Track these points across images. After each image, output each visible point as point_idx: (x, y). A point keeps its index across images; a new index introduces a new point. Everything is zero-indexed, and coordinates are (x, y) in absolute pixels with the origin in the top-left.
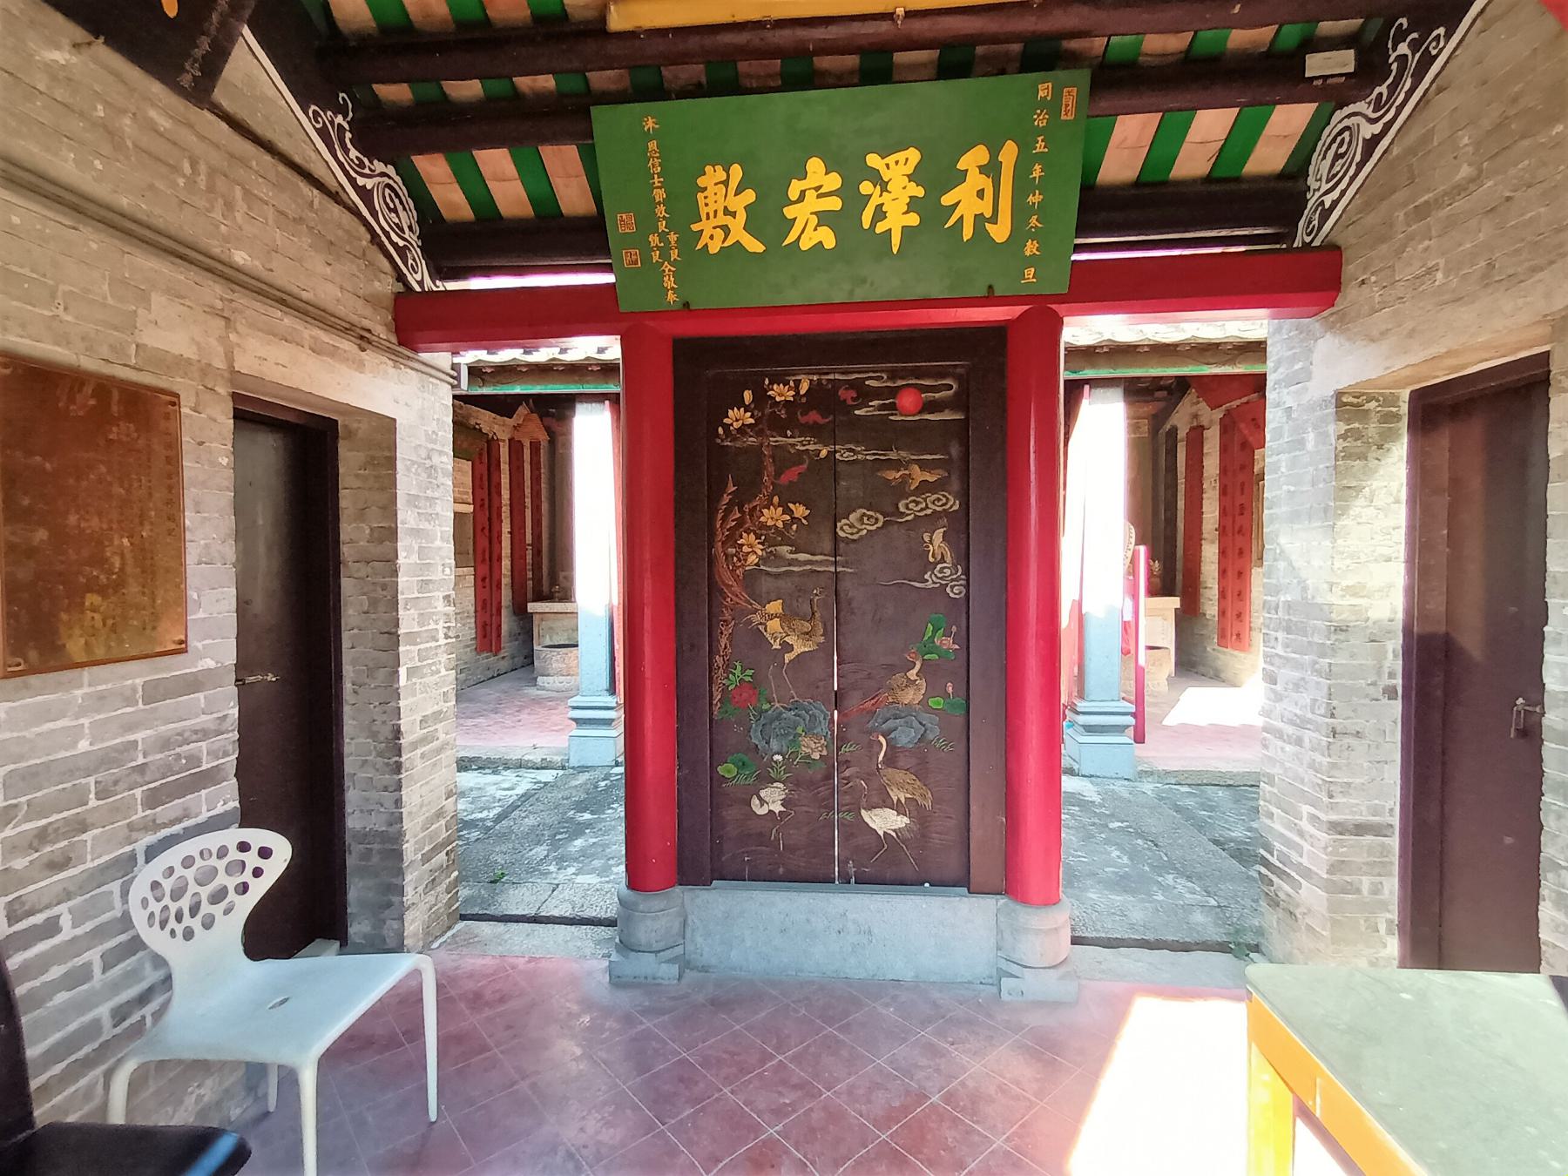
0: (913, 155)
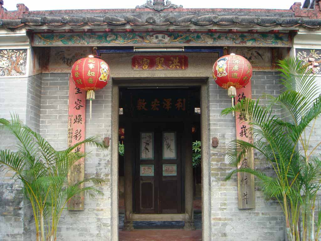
0: (171, 99)
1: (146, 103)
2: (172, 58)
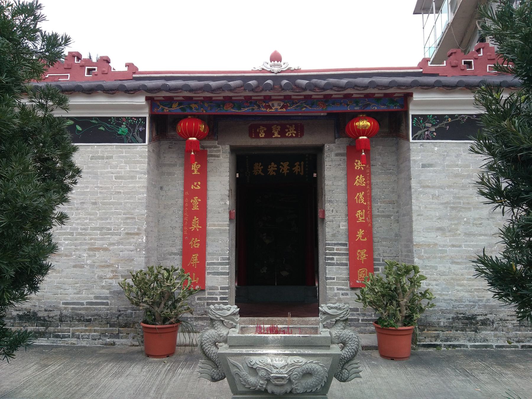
1: (262, 167)
2: (288, 126)
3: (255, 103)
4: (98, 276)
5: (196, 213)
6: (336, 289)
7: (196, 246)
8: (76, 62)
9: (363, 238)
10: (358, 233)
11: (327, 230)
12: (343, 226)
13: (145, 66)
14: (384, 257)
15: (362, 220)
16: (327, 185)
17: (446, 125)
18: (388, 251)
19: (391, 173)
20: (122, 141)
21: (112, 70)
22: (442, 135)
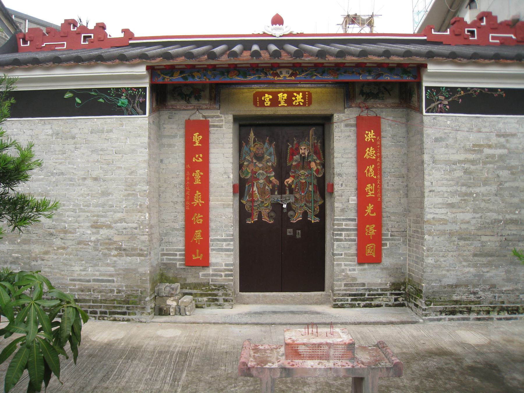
2: (295, 94)
3: (262, 71)
4: (102, 254)
5: (198, 187)
6: (343, 265)
7: (199, 221)
8: (72, 30)
9: (372, 213)
10: (368, 207)
11: (336, 205)
12: (353, 200)
13: (142, 30)
14: (392, 232)
15: (372, 194)
16: (340, 175)
17: (459, 98)
18: (396, 227)
19: (401, 146)
20: (122, 113)
21: (108, 37)
22: (455, 108)
